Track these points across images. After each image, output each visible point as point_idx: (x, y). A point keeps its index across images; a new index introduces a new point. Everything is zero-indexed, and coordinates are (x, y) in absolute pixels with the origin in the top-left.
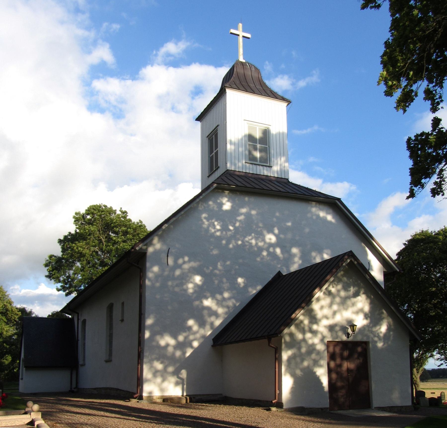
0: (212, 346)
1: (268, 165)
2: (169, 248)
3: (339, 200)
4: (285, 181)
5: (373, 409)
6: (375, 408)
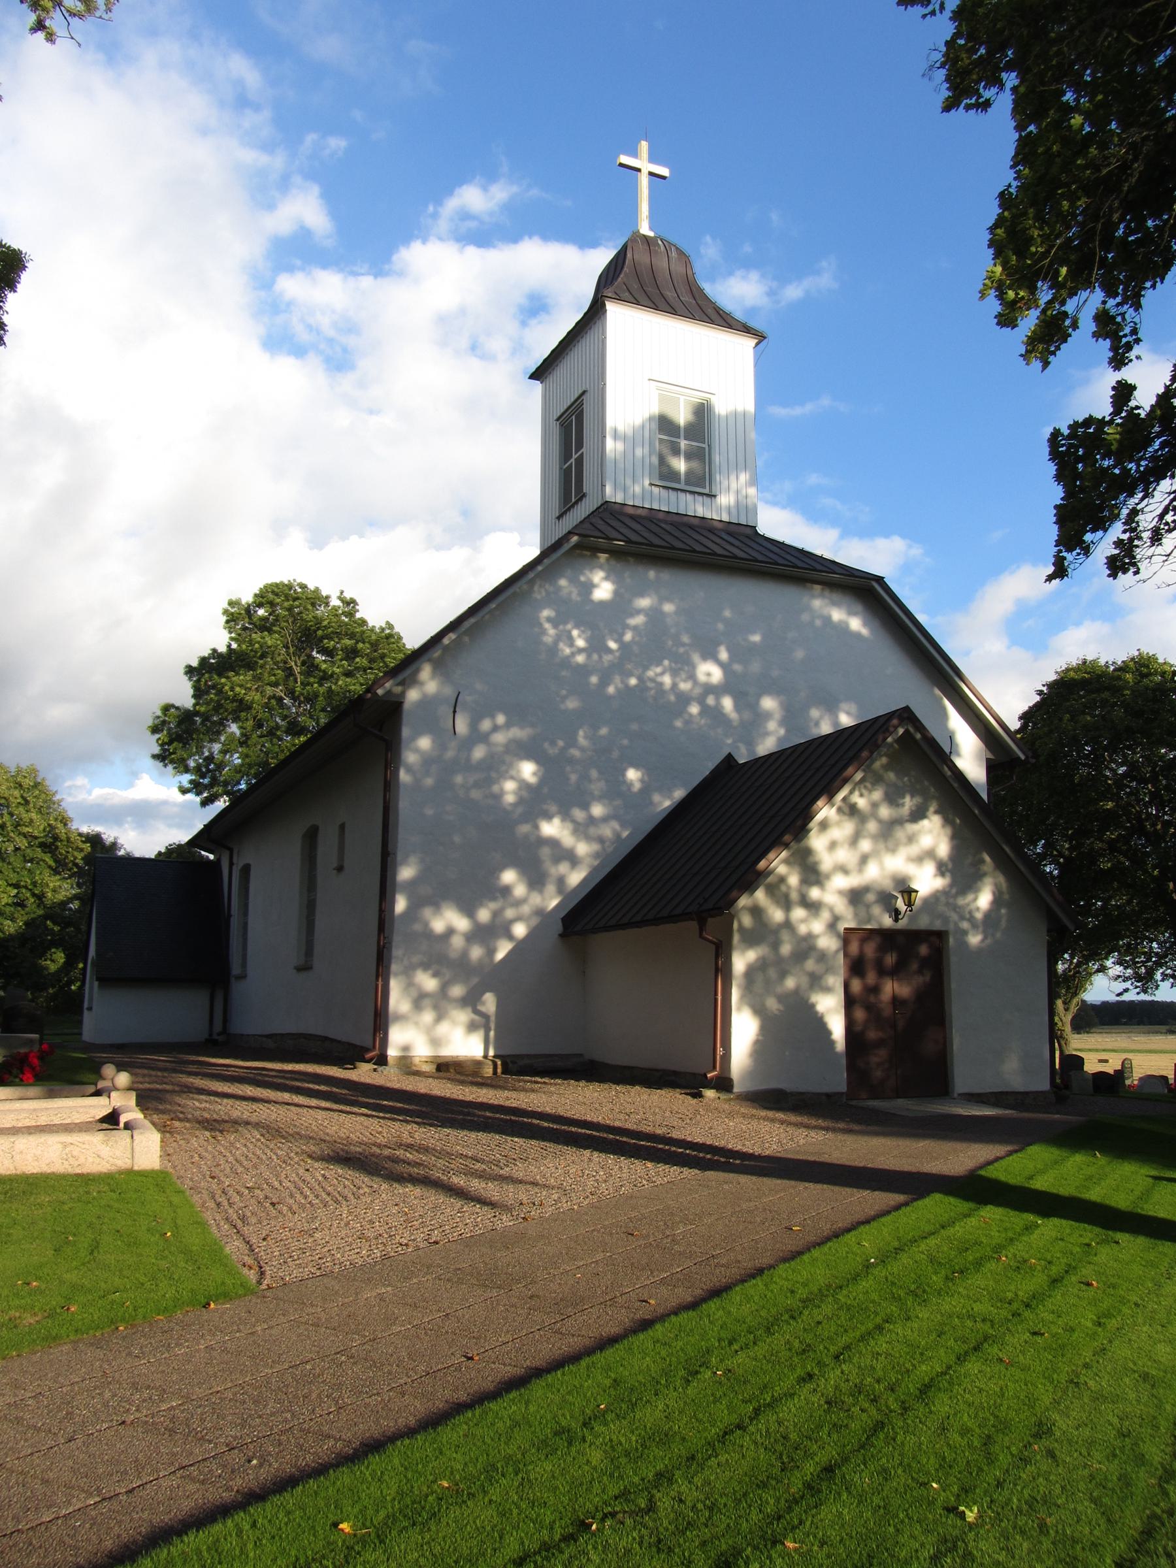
0: (560, 935)
1: (706, 491)
3: (880, 580)
4: (748, 531)
6: (959, 1095)
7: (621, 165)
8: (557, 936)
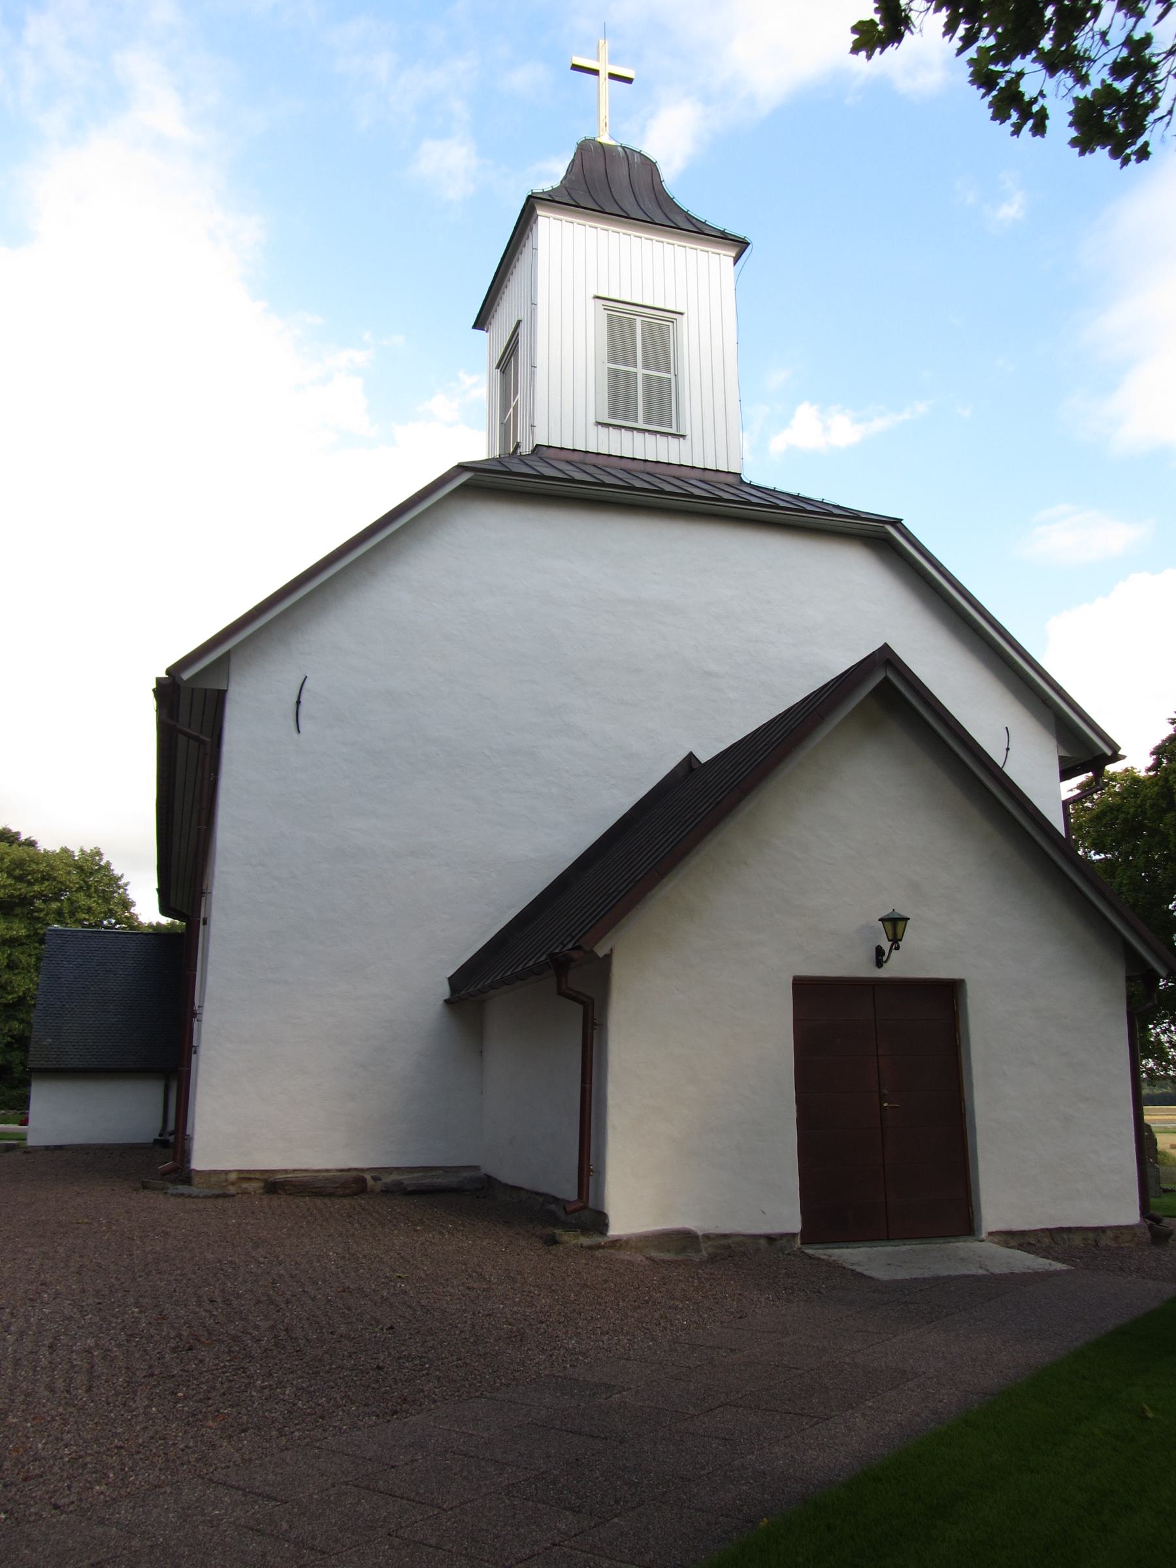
0: (446, 1001)
1: (673, 431)
2: (306, 677)
3: (896, 523)
4: (731, 479)
5: (983, 1241)
6: (990, 1234)
7: (575, 67)
8: (441, 1002)
